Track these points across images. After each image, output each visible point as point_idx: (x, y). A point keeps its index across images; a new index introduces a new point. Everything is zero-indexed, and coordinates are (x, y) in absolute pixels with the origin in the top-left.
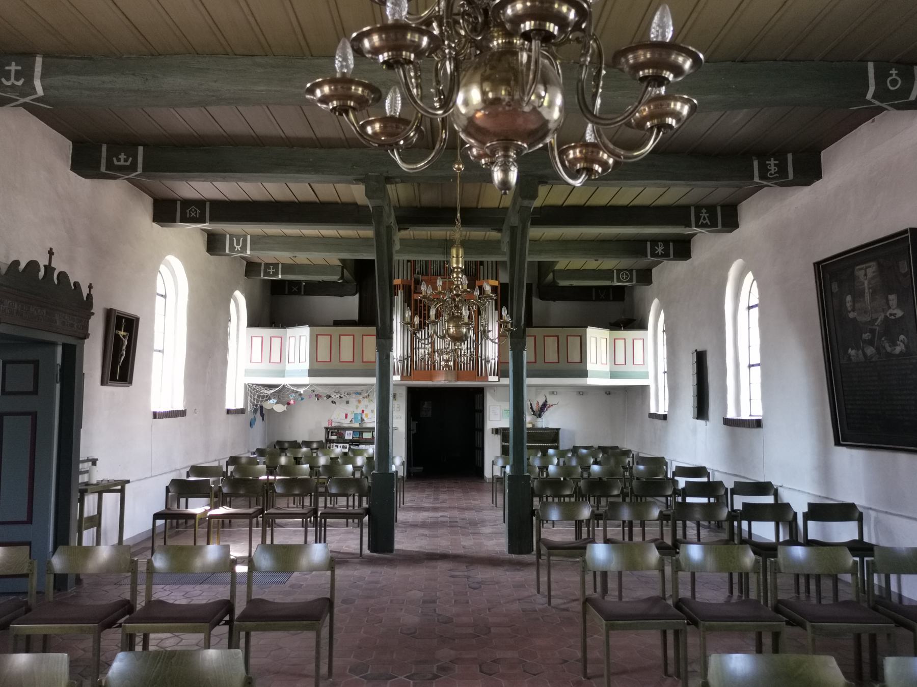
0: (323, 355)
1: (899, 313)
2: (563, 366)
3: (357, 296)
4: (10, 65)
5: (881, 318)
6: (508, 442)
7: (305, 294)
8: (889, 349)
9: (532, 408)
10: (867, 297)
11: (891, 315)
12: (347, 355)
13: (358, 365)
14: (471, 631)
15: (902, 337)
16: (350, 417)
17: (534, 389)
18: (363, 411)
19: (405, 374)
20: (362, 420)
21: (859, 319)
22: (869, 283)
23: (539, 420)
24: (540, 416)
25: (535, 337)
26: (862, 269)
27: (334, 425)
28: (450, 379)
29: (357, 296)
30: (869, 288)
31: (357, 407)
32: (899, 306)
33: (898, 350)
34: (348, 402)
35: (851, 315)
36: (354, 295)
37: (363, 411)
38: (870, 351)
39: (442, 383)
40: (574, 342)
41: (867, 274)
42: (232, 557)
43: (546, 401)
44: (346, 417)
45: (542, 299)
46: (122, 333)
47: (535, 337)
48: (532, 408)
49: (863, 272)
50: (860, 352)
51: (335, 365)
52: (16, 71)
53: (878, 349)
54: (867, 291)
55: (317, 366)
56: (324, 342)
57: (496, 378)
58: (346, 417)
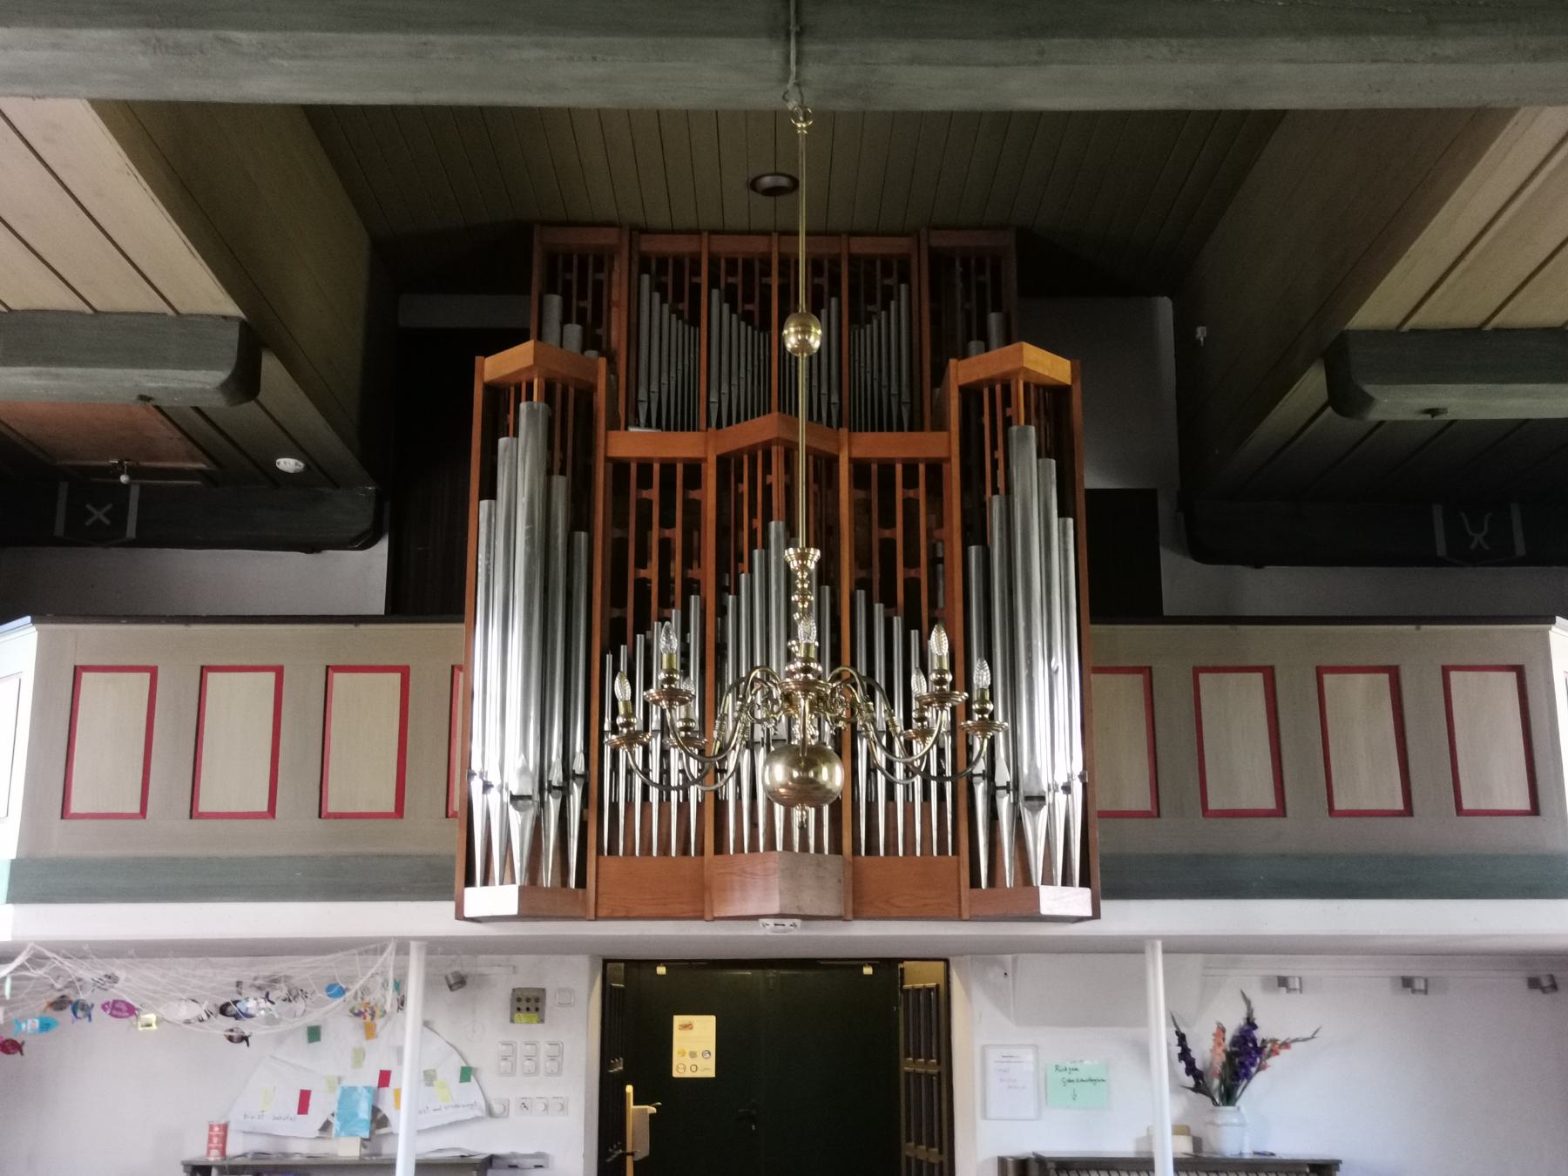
0: (106, 778)
2: (1431, 830)
3: (382, 548)
4: (98, 506)
7: (143, 541)
9: (1185, 1055)
12: (235, 778)
13: (295, 832)
14: (560, 484)
16: (321, 1107)
17: (1194, 962)
18: (385, 1078)
19: (547, 878)
20: (379, 1120)
23: (1227, 1114)
24: (1229, 1097)
25: (1269, 674)
27: (238, 1147)
28: (810, 905)
29: (382, 548)
31: (359, 1057)
34: (314, 1034)
36: (365, 541)
37: (385, 1078)
39: (766, 929)
40: (1486, 704)
43: (1251, 1024)
44: (303, 1108)
45: (1202, 553)
47: (1269, 674)
48: (1185, 1055)
51: (168, 834)
55: (66, 842)
56: (112, 705)
57: (1076, 900)
58: (303, 1108)
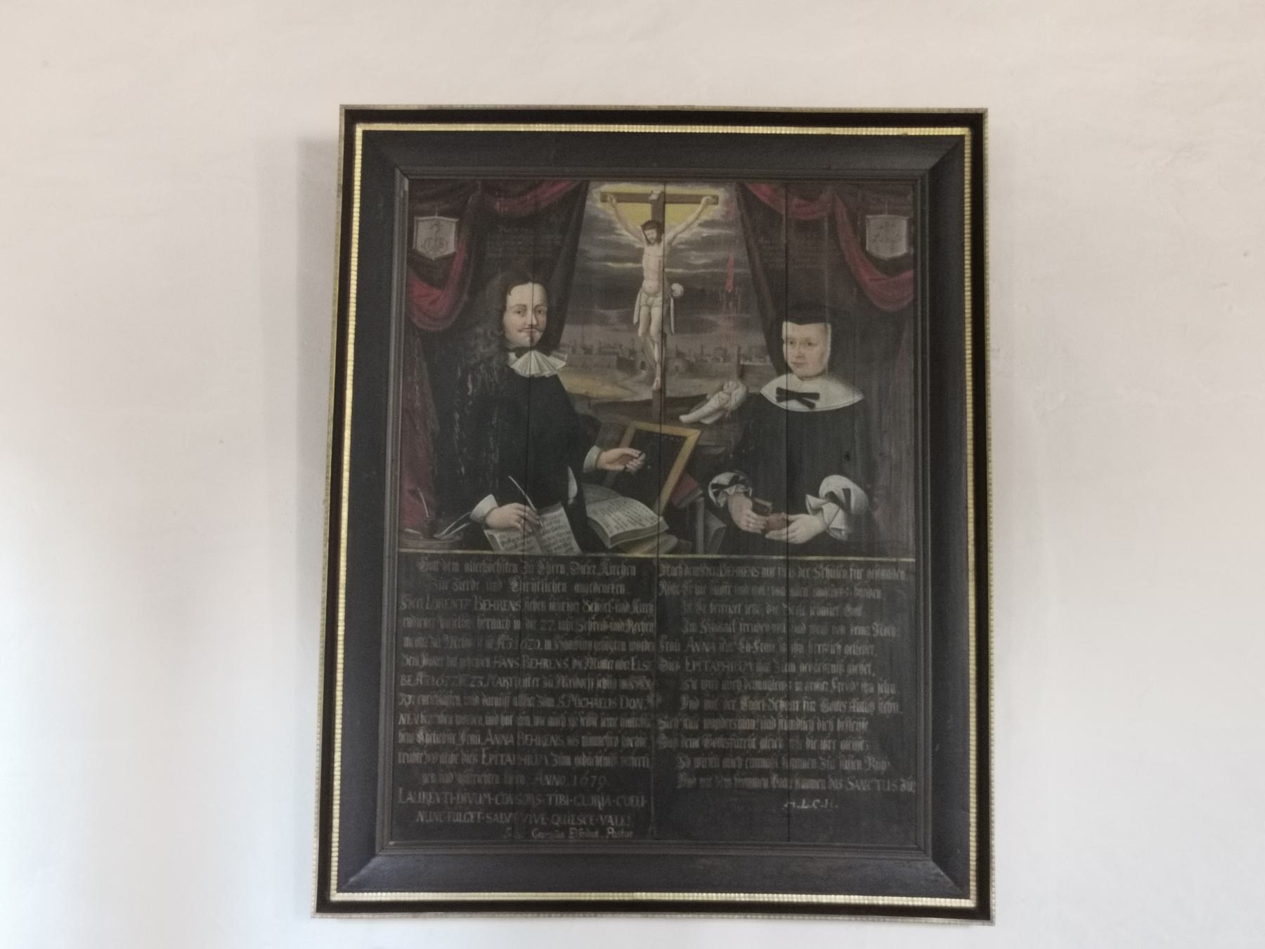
1: (836, 396)
5: (732, 394)
6: (701, 197)
8: (746, 516)
10: (650, 308)
11: (784, 394)
15: (834, 483)
21: (572, 384)
22: (673, 255)
26: (641, 198)
30: (667, 279)
32: (836, 368)
33: (803, 527)
35: (528, 365)
38: (620, 518)
41: (661, 231)
42: (455, 220)
46: (761, 240)
49: (644, 212)
50: (559, 516)
52: (736, 275)
53: (678, 520)
54: (650, 283)
